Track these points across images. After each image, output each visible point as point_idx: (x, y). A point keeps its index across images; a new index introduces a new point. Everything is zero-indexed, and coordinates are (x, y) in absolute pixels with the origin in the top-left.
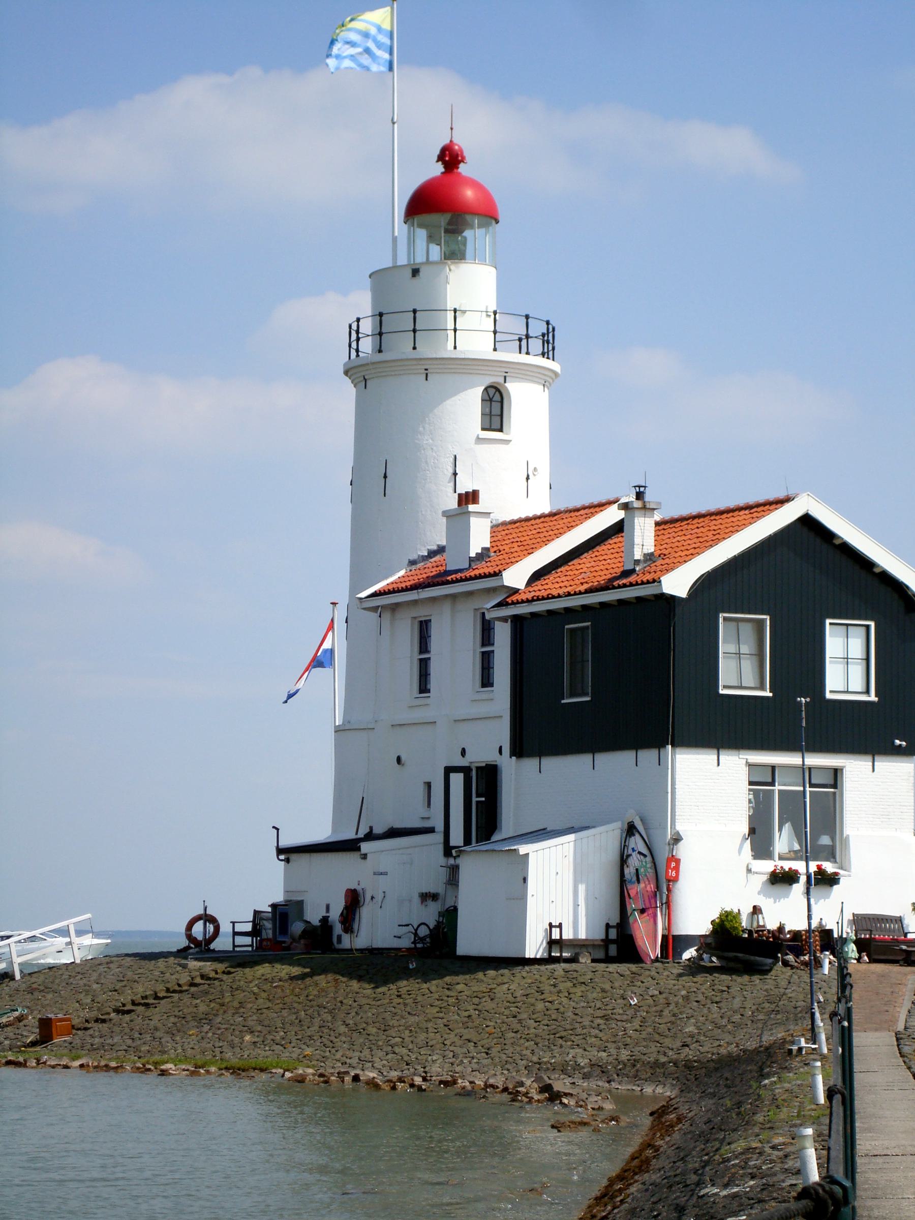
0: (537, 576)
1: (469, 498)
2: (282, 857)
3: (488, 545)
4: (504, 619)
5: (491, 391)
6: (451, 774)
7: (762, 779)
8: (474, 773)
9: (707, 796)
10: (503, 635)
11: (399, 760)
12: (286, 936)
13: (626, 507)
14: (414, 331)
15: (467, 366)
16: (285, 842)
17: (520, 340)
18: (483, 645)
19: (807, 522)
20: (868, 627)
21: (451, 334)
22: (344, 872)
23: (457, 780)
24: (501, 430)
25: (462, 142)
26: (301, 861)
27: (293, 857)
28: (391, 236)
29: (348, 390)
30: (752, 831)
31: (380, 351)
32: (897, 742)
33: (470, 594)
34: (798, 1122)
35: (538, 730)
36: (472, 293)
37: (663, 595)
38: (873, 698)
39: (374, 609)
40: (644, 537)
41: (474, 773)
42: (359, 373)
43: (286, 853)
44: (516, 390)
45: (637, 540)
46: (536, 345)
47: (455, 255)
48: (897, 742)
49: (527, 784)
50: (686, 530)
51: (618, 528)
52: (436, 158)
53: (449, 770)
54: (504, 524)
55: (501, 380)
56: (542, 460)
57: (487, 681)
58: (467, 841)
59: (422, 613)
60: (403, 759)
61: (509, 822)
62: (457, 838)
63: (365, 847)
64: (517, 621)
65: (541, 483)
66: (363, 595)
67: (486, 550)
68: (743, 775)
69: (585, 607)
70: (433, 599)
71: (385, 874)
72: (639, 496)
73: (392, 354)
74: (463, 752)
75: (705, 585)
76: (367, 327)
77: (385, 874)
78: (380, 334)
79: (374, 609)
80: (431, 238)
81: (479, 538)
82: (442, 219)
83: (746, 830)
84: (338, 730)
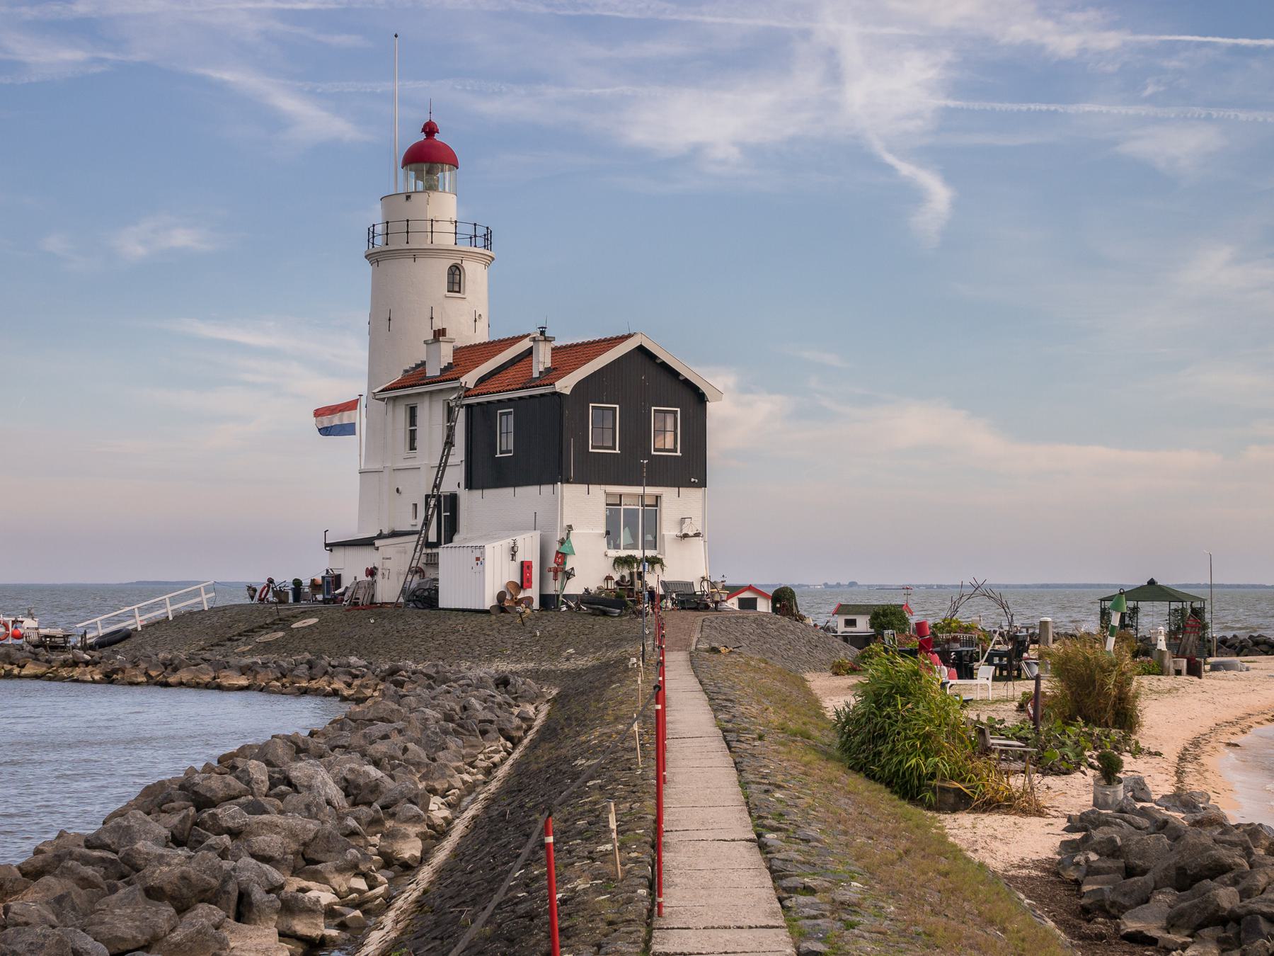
0: (482, 380)
1: (440, 334)
6: (441, 606)
7: (613, 505)
9: (582, 510)
10: (461, 415)
13: (534, 340)
19: (641, 349)
22: (367, 558)
26: (339, 552)
29: (367, 268)
30: (608, 533)
33: (441, 391)
35: (487, 471)
36: (445, 207)
37: (555, 393)
39: (383, 400)
46: (480, 241)
47: (431, 187)
49: (474, 505)
50: (568, 356)
51: (529, 352)
53: (427, 497)
54: (461, 348)
56: (483, 310)
59: (411, 402)
63: (377, 543)
64: (469, 406)
65: (483, 325)
68: (602, 500)
69: (510, 400)
70: (419, 394)
72: (542, 333)
76: (379, 229)
79: (383, 400)
80: (417, 178)
81: (446, 354)
82: (425, 167)
83: (603, 531)
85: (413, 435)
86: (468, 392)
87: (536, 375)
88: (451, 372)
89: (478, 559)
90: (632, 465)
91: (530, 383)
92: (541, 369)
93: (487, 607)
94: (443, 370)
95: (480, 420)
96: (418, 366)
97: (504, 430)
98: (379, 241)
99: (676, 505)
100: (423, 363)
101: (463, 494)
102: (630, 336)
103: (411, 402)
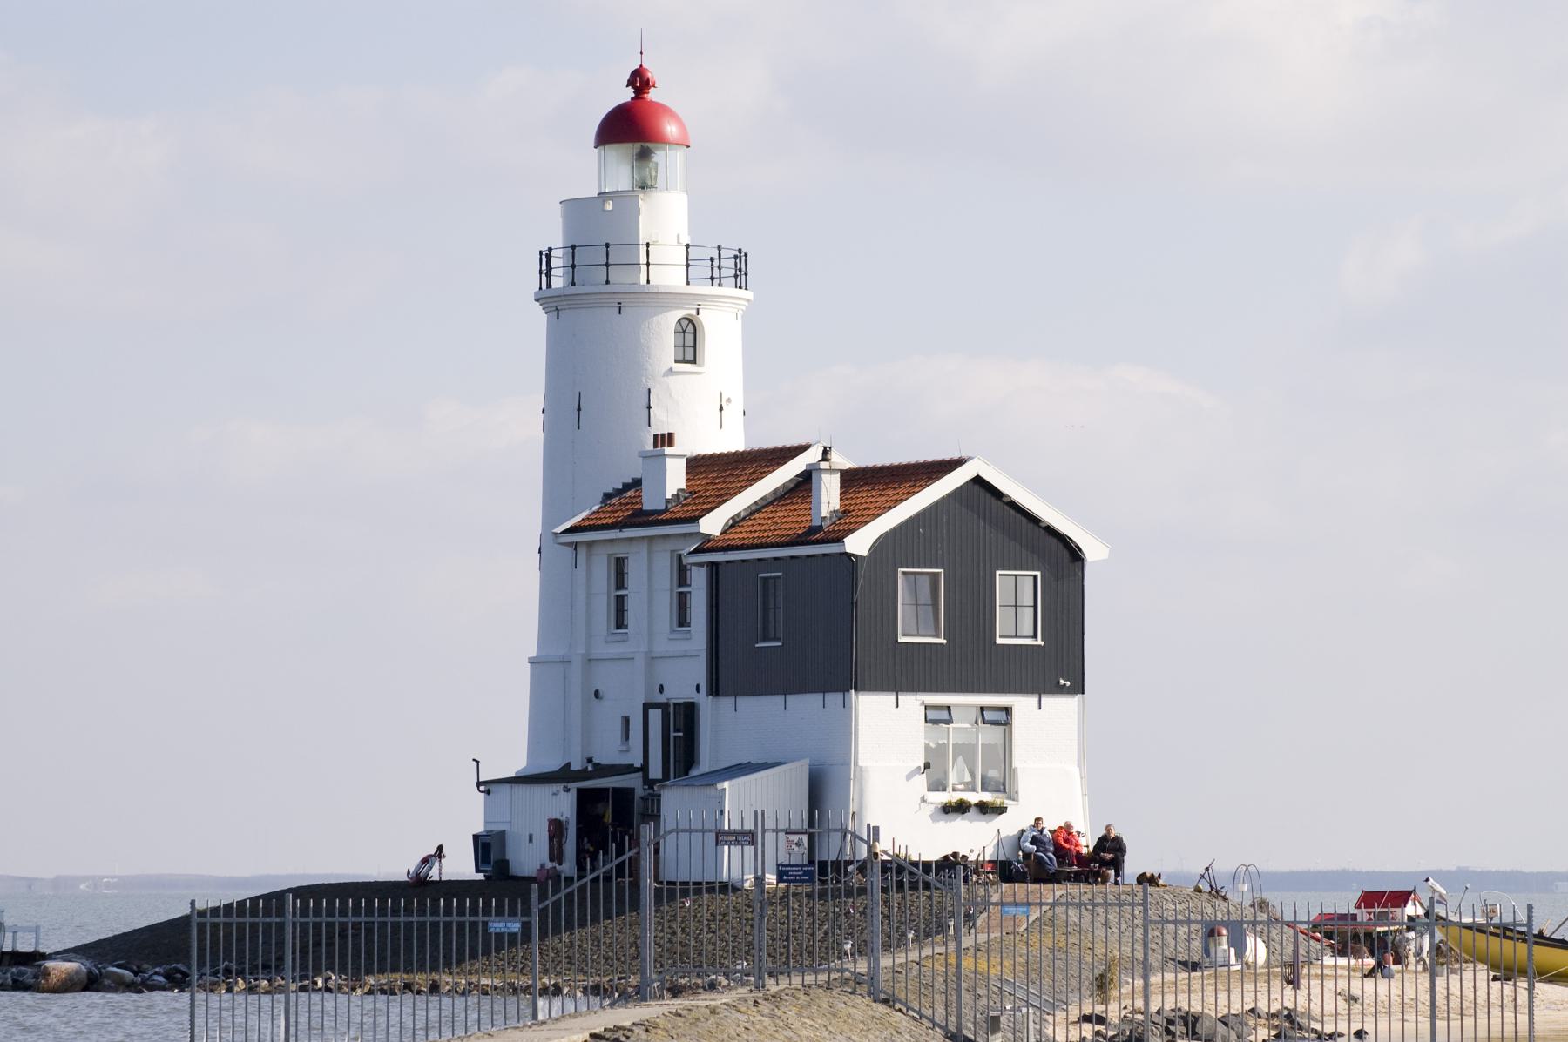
1: (666, 439)
4: (701, 565)
5: (685, 323)
8: (672, 710)
11: (597, 694)
14: (607, 265)
15: (663, 300)
17: (712, 259)
18: (680, 585)
19: (978, 481)
20: (1035, 577)
21: (644, 268)
23: (656, 716)
24: (694, 362)
25: (653, 73)
27: (493, 788)
28: (590, 170)
31: (573, 284)
38: (1040, 642)
40: (829, 496)
41: (672, 710)
42: (551, 302)
43: (487, 787)
44: (707, 318)
45: (824, 499)
49: (728, 725)
53: (647, 707)
55: (694, 312)
57: (683, 621)
58: (666, 776)
59: (620, 551)
61: (705, 763)
62: (655, 771)
64: (714, 567)
65: (734, 413)
66: (559, 529)
70: (631, 539)
73: (588, 281)
74: (661, 689)
75: (884, 544)
78: (573, 266)
84: (532, 662)
85: (620, 605)
86: (707, 545)
90: (965, 661)
91: (811, 535)
93: (415, 816)
96: (627, 487)
98: (558, 282)
99: (1042, 722)
100: (637, 483)
101: (705, 703)
102: (959, 462)
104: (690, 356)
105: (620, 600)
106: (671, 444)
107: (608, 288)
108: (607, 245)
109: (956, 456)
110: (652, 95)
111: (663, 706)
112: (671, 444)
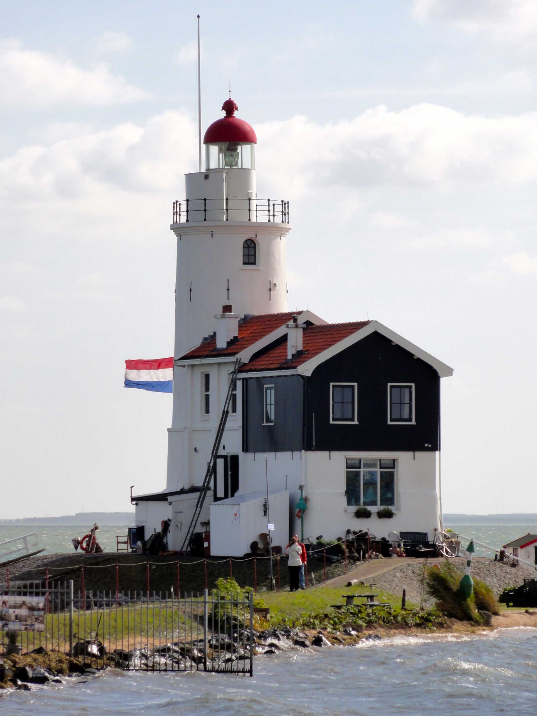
2: (134, 502)
3: (237, 335)
5: (249, 242)
8: (229, 459)
9: (323, 473)
10: (239, 384)
11: (195, 450)
12: (147, 545)
16: (136, 494)
22: (164, 511)
23: (220, 463)
24: (254, 263)
26: (142, 503)
27: (140, 503)
32: (426, 445)
34: (456, 649)
35: (262, 438)
41: (229, 459)
48: (426, 445)
49: (252, 466)
52: (221, 108)
55: (254, 236)
59: (207, 370)
60: (197, 449)
62: (221, 493)
67: (235, 337)
71: (182, 512)
77: (182, 512)
84: (169, 430)
87: (290, 357)
88: (235, 345)
89: (236, 515)
90: (376, 432)
92: (294, 352)
94: (229, 344)
95: (250, 398)
97: (269, 403)
103: (207, 370)
104: (252, 261)
105: (207, 397)
106: (230, 311)
107: (228, 223)
108: (205, 200)
109: (366, 320)
110: (237, 114)
111: (225, 457)
112: (230, 311)
